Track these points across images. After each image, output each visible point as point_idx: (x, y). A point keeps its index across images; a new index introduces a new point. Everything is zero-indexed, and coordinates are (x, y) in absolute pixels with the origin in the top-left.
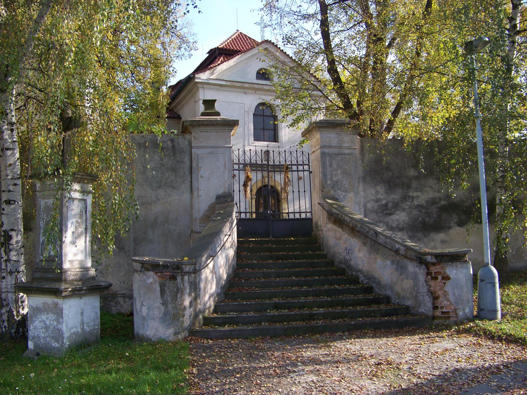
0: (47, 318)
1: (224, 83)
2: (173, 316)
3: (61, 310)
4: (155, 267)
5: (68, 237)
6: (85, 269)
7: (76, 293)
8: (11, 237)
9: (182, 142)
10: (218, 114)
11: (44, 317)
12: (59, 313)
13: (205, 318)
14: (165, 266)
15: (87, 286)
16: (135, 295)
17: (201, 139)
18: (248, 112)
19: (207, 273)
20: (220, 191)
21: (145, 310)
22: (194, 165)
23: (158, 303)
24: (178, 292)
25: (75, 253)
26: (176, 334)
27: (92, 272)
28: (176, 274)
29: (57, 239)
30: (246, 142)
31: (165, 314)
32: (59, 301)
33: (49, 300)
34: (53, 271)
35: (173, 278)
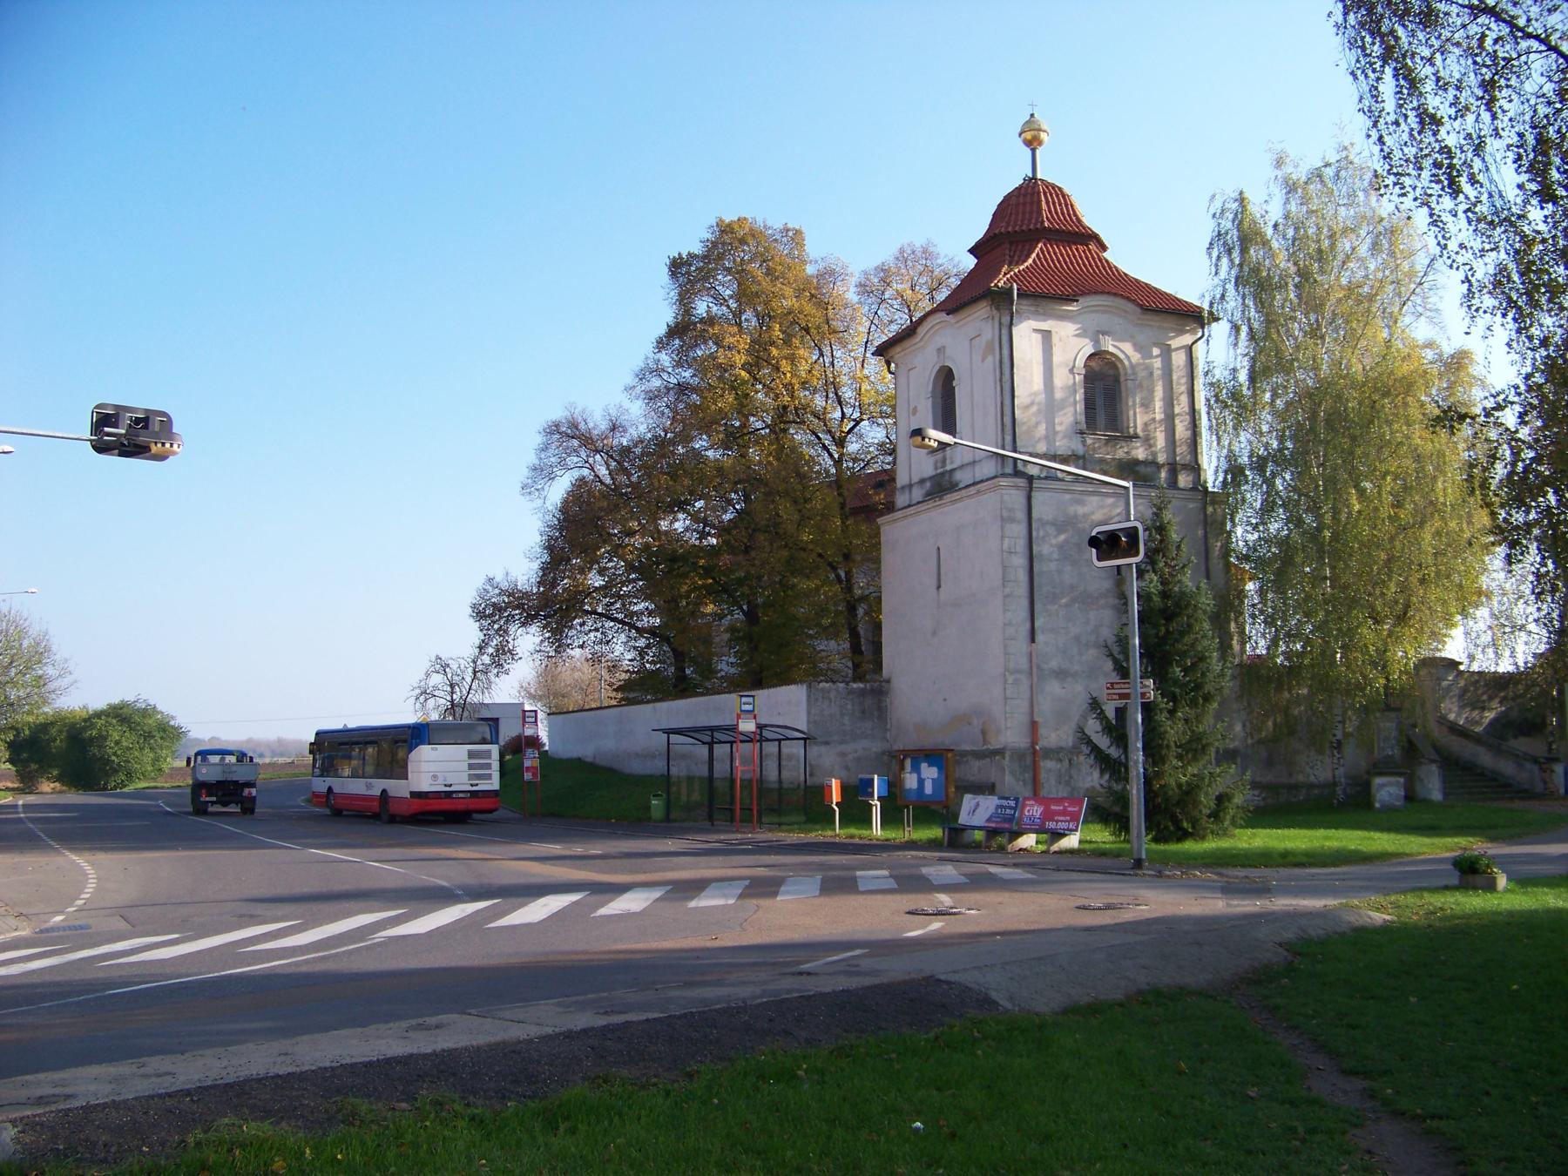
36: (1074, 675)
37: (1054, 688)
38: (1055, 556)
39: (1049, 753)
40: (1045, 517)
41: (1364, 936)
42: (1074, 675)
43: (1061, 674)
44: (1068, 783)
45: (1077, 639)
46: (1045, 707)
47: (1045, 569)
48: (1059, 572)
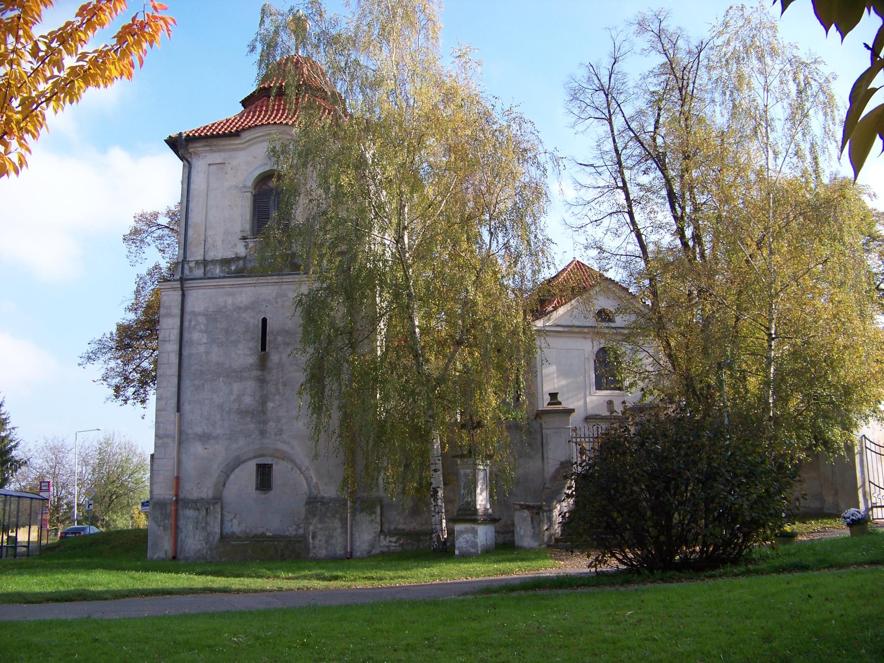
0: (468, 536)
1: (561, 329)
2: (537, 535)
3: (477, 531)
4: (528, 507)
5: (478, 491)
6: (486, 510)
7: (485, 522)
8: (437, 492)
9: (536, 425)
10: (560, 403)
11: (465, 536)
12: (475, 533)
13: (556, 539)
14: (533, 507)
15: (490, 519)
16: (516, 523)
17: (549, 423)
18: (588, 359)
19: (556, 512)
20: (563, 459)
21: (522, 532)
22: (544, 441)
23: (530, 527)
24: (540, 522)
25: (482, 500)
26: (540, 545)
27: (490, 511)
28: (539, 511)
29: (473, 493)
30: (588, 392)
31: (534, 534)
32: (475, 526)
33: (468, 526)
34: (470, 510)
35: (538, 513)
36: (216, 438)
37: (198, 448)
38: (205, 340)
39: (195, 504)
40: (197, 310)
41: (108, 567)
42: (216, 438)
43: (205, 438)
44: (204, 529)
45: (221, 407)
46: (190, 465)
47: (194, 351)
48: (207, 353)
